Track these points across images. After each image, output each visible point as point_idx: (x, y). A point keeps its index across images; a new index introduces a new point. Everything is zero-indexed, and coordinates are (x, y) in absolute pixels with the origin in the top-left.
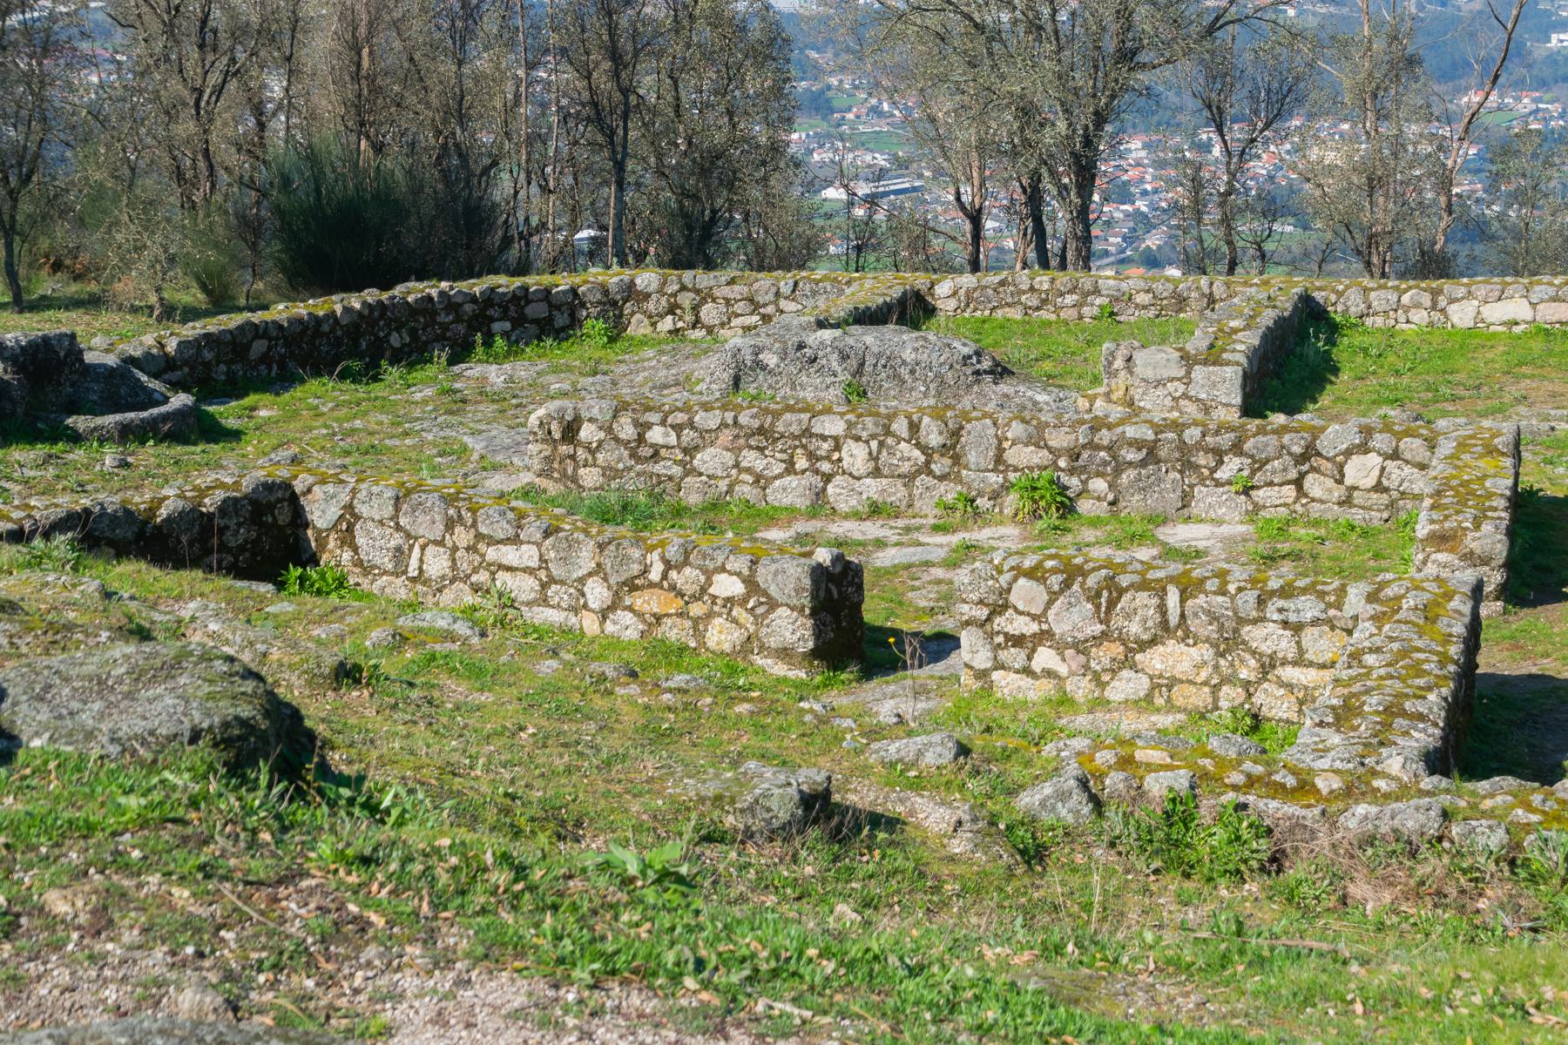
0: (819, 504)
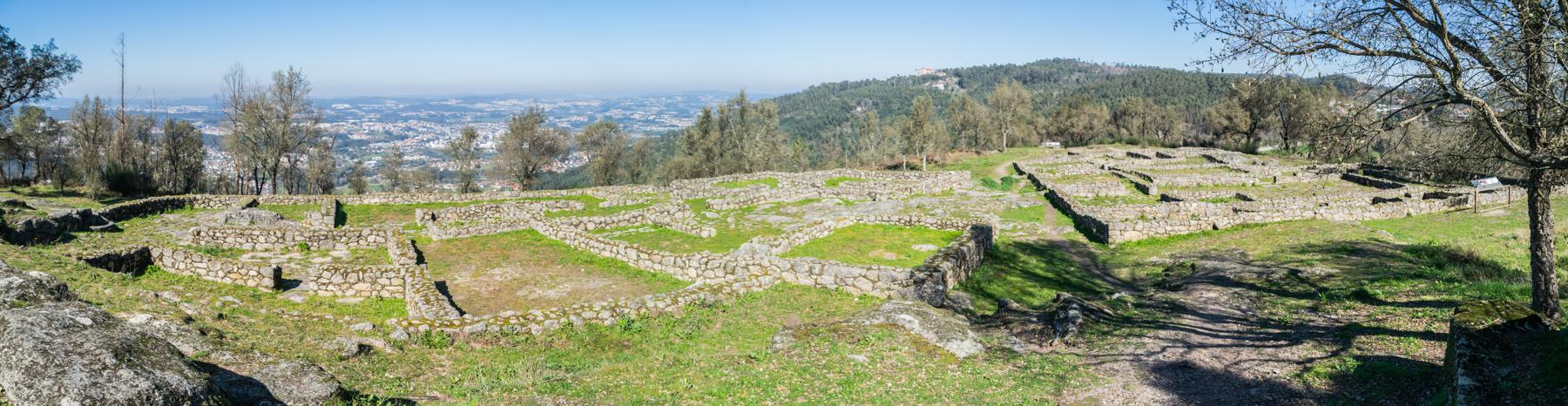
0: (254, 249)
